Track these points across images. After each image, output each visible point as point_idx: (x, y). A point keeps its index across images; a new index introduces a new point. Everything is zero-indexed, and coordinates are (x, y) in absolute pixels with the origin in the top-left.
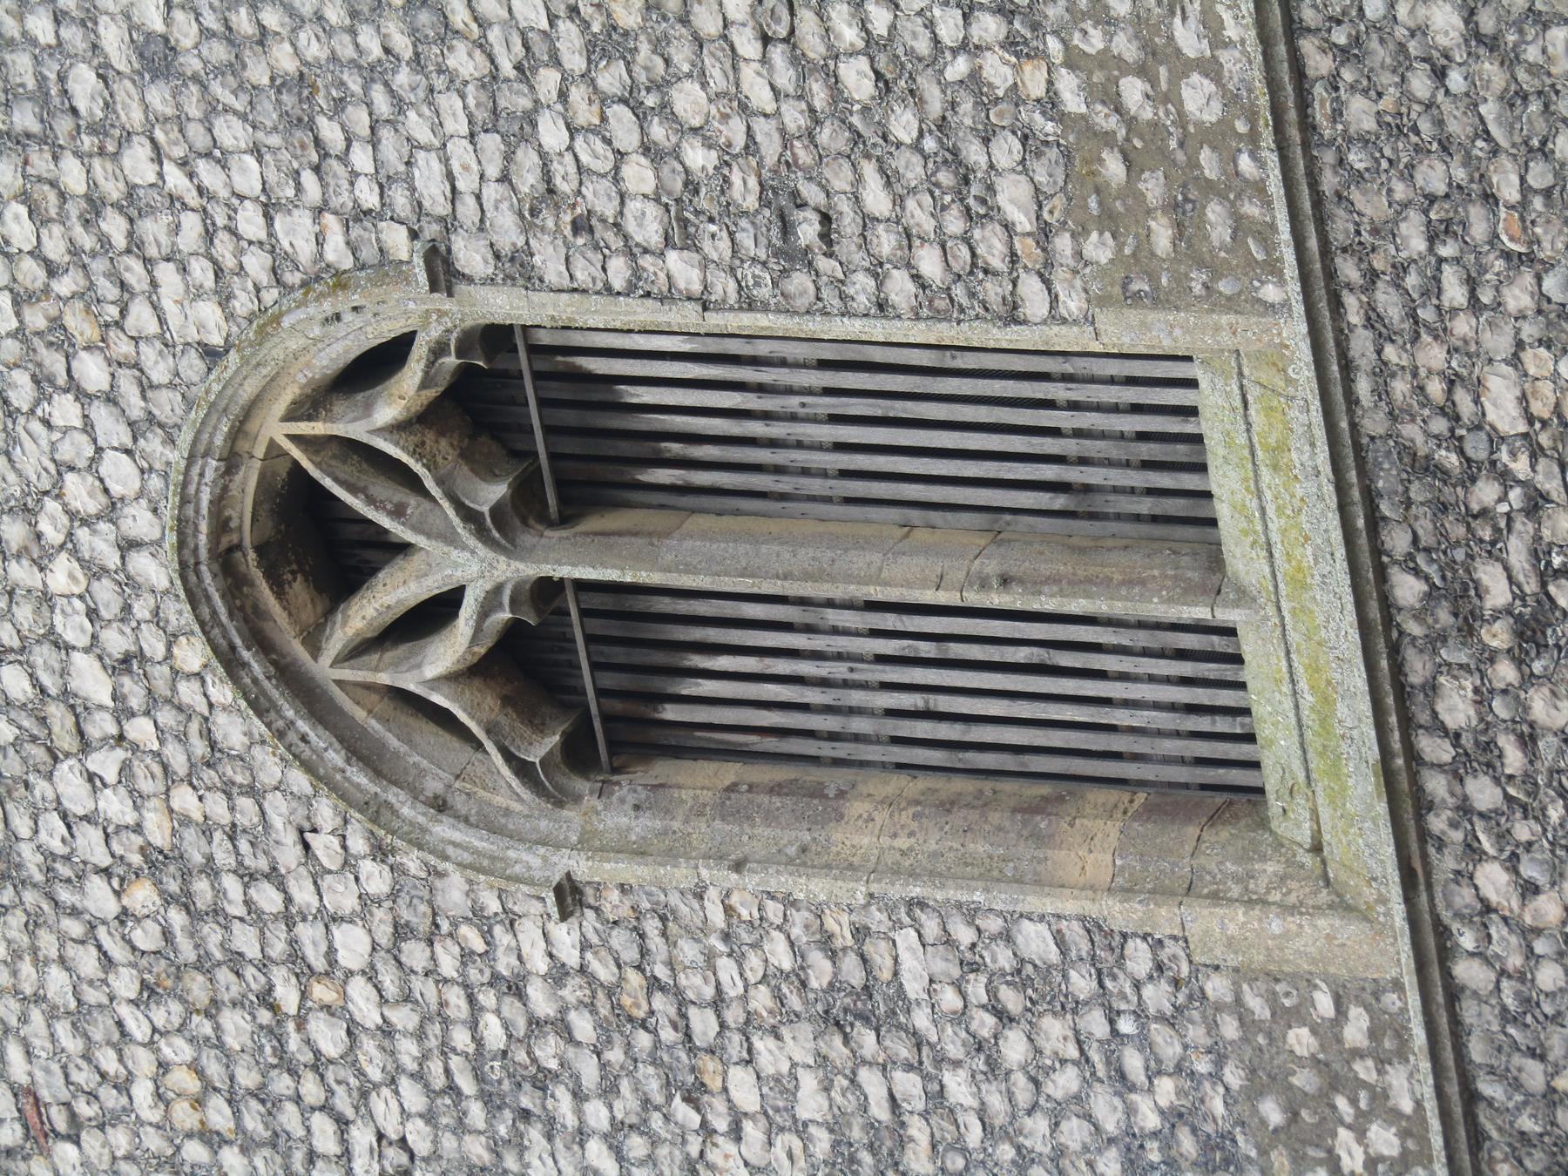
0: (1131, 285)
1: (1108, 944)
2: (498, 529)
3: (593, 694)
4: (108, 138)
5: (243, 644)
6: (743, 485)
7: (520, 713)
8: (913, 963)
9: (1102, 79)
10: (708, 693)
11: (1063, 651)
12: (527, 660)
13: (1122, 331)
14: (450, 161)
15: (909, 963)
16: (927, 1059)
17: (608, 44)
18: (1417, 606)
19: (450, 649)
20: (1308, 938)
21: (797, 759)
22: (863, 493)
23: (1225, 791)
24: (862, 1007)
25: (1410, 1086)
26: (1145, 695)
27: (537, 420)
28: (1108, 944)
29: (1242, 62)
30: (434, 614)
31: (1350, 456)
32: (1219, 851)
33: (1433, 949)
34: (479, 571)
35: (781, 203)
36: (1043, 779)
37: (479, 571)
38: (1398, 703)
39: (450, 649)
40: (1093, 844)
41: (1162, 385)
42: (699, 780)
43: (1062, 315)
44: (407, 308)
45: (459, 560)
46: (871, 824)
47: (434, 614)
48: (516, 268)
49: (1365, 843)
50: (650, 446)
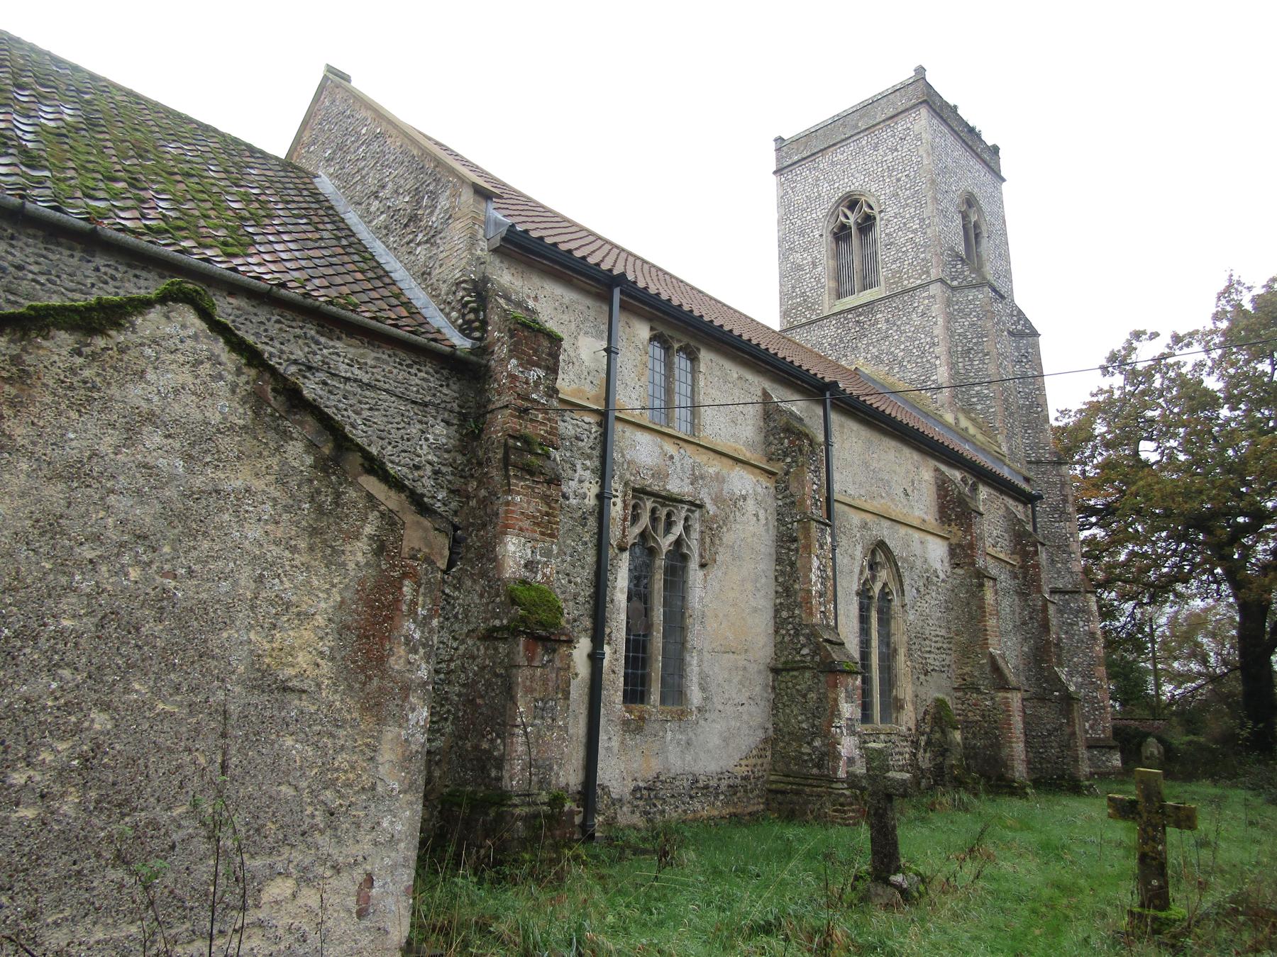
0: (887, 278)
1: (823, 287)
2: (856, 222)
3: (841, 234)
4: (891, 176)
5: (842, 199)
6: (863, 245)
7: (420, 859)
8: (820, 269)
9: (907, 273)
10: (843, 245)
11: (851, 278)
12: (844, 227)
13: (882, 279)
14: (891, 212)
15: (180, 810)
16: (810, 272)
17: (905, 224)
18: (1069, 388)
19: (844, 220)
20: (826, 306)
21: (837, 255)
22: (863, 257)
23: (839, 296)
24: (814, 265)
25: (814, 317)
26: (847, 286)
27: (867, 223)
28: (823, 287)
29: (910, 286)
30: (847, 217)
31: (873, 302)
32: (833, 296)
33: (827, 317)
34: (852, 221)
35: (891, 244)
36: (838, 279)
37: (852, 221)
38: (849, 311)
39: (844, 220)
40: (833, 284)
41: (877, 283)
42: (834, 245)
43: (883, 273)
44: (876, 209)
45: (852, 219)
46: (832, 263)
47: (847, 217)
48: (882, 219)
49: (836, 310)
50: (866, 235)
